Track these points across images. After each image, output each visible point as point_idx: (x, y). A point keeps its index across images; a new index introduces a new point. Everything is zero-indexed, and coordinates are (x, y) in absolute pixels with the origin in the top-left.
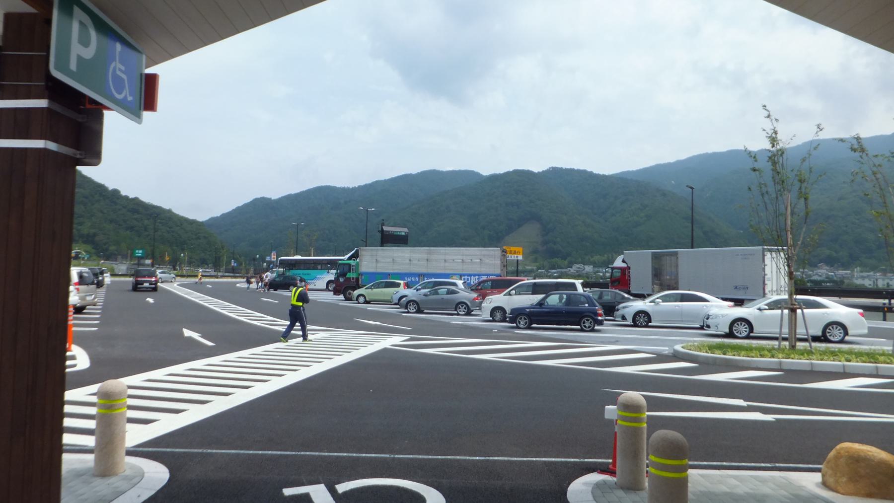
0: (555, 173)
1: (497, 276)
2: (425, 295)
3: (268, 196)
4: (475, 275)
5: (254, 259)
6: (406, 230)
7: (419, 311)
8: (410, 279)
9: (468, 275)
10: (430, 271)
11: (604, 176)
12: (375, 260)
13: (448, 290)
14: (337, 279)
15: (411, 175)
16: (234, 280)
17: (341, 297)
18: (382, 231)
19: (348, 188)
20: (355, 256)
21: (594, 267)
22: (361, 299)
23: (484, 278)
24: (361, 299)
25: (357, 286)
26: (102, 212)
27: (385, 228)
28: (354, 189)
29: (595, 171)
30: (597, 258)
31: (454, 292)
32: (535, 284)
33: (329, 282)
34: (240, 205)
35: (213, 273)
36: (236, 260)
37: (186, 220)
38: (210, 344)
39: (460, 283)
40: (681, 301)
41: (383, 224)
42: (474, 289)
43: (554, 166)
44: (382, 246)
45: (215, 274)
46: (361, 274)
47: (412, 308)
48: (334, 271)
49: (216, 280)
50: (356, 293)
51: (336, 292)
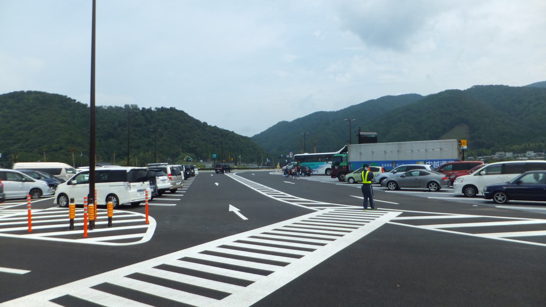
0: (478, 90)
1: (455, 160)
2: (402, 176)
3: (286, 120)
4: (436, 161)
5: (280, 158)
6: (375, 133)
7: (397, 189)
8: (385, 165)
9: (431, 161)
10: (401, 159)
11: (518, 88)
12: (358, 153)
13: (421, 172)
14: (333, 167)
15: (373, 100)
16: (268, 170)
17: (337, 179)
18: (359, 135)
19: (334, 112)
20: (345, 150)
21: (514, 153)
22: (351, 181)
23: (444, 163)
24: (351, 181)
25: (348, 172)
26: (199, 135)
27: (361, 133)
28: (338, 112)
29: (511, 85)
30: (515, 147)
31: (422, 174)
32: (504, 165)
33: (327, 170)
34: (271, 126)
35: (257, 166)
36: (269, 158)
37: (242, 137)
38: (244, 218)
39: (428, 167)
40: (503, 173)
41: (360, 131)
42: (440, 170)
43: (476, 84)
44: (360, 143)
45: (257, 166)
46: (350, 163)
47: (392, 186)
48: (331, 162)
49: (258, 170)
50: (347, 176)
51: (333, 176)
